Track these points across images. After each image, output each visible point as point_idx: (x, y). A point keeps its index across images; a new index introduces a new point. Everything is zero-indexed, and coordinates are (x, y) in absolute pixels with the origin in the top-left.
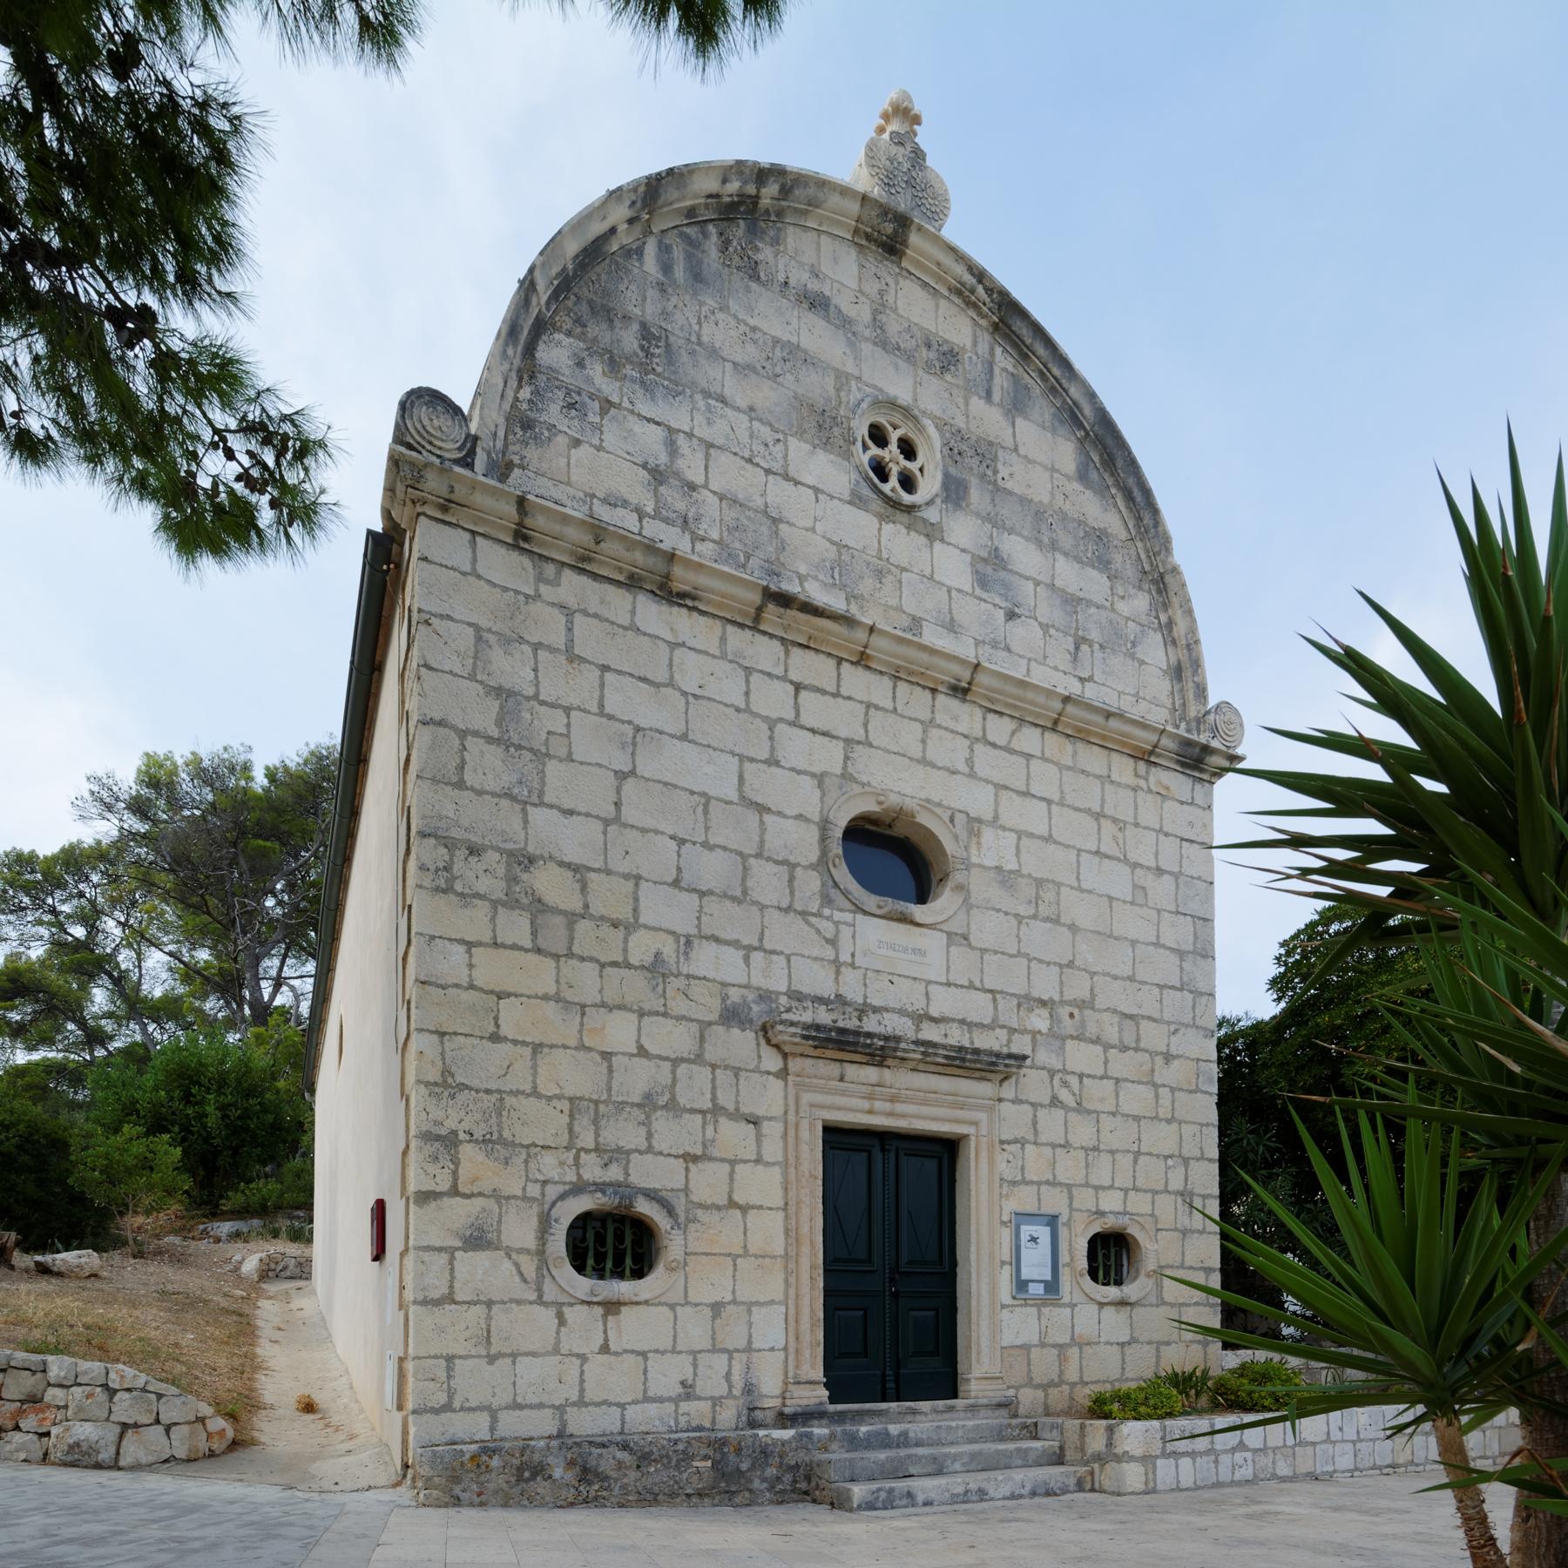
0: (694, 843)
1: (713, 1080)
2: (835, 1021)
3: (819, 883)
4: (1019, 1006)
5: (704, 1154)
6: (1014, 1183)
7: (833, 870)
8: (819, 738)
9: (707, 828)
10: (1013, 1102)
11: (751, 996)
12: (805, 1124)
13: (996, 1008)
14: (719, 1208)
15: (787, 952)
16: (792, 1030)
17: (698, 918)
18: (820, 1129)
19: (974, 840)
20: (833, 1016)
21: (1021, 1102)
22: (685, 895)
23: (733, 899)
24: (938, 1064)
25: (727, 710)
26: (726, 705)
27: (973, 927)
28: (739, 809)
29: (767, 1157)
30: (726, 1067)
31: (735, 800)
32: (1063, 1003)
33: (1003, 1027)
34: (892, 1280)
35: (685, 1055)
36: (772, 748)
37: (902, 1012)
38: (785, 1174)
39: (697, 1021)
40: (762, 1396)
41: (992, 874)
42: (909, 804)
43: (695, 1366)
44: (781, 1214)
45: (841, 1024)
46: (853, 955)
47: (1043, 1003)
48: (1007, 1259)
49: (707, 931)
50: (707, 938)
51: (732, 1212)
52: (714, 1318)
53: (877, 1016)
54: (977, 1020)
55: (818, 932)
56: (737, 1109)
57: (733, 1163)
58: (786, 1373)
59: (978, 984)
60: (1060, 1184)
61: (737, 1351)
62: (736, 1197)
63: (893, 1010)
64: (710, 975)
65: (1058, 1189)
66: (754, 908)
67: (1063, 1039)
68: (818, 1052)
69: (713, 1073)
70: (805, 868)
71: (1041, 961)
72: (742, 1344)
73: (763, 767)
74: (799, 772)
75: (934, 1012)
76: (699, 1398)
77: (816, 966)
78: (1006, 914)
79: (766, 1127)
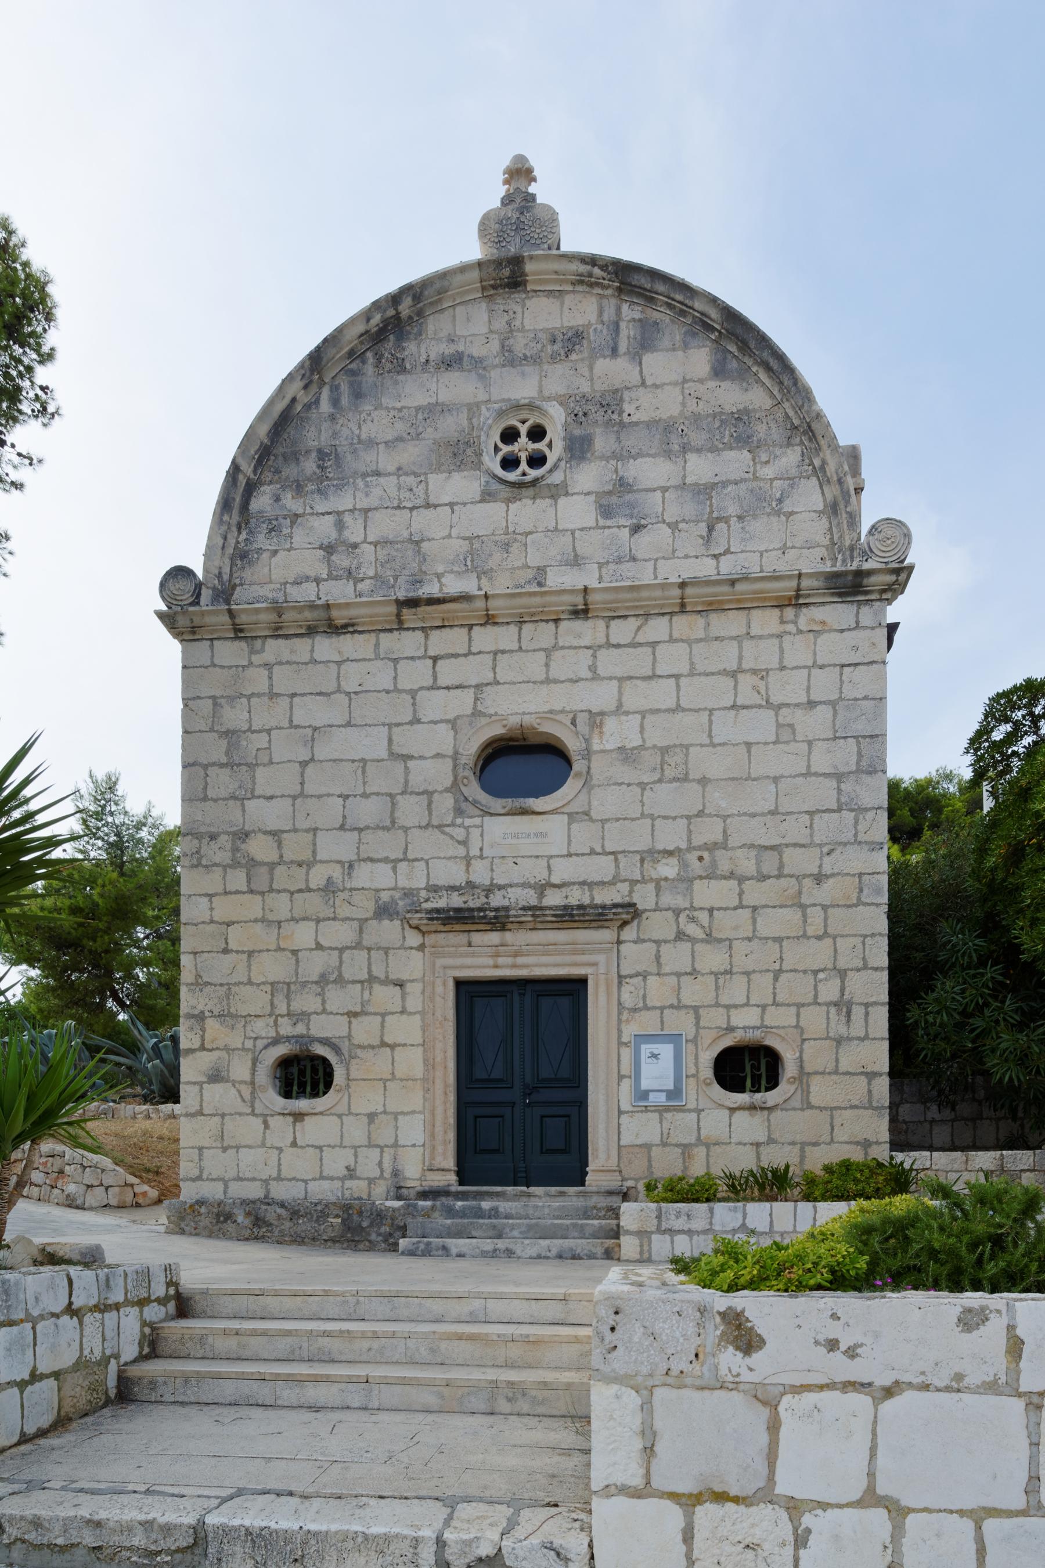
2: (465, 902)
14: (373, 1047)
16: (418, 915)
30: (379, 949)
37: (525, 885)
47: (670, 853)
50: (364, 860)
52: (369, 1124)
54: (597, 878)
55: (452, 837)
60: (685, 1007)
61: (387, 1146)
72: (391, 1141)
74: (435, 723)
76: (359, 1178)
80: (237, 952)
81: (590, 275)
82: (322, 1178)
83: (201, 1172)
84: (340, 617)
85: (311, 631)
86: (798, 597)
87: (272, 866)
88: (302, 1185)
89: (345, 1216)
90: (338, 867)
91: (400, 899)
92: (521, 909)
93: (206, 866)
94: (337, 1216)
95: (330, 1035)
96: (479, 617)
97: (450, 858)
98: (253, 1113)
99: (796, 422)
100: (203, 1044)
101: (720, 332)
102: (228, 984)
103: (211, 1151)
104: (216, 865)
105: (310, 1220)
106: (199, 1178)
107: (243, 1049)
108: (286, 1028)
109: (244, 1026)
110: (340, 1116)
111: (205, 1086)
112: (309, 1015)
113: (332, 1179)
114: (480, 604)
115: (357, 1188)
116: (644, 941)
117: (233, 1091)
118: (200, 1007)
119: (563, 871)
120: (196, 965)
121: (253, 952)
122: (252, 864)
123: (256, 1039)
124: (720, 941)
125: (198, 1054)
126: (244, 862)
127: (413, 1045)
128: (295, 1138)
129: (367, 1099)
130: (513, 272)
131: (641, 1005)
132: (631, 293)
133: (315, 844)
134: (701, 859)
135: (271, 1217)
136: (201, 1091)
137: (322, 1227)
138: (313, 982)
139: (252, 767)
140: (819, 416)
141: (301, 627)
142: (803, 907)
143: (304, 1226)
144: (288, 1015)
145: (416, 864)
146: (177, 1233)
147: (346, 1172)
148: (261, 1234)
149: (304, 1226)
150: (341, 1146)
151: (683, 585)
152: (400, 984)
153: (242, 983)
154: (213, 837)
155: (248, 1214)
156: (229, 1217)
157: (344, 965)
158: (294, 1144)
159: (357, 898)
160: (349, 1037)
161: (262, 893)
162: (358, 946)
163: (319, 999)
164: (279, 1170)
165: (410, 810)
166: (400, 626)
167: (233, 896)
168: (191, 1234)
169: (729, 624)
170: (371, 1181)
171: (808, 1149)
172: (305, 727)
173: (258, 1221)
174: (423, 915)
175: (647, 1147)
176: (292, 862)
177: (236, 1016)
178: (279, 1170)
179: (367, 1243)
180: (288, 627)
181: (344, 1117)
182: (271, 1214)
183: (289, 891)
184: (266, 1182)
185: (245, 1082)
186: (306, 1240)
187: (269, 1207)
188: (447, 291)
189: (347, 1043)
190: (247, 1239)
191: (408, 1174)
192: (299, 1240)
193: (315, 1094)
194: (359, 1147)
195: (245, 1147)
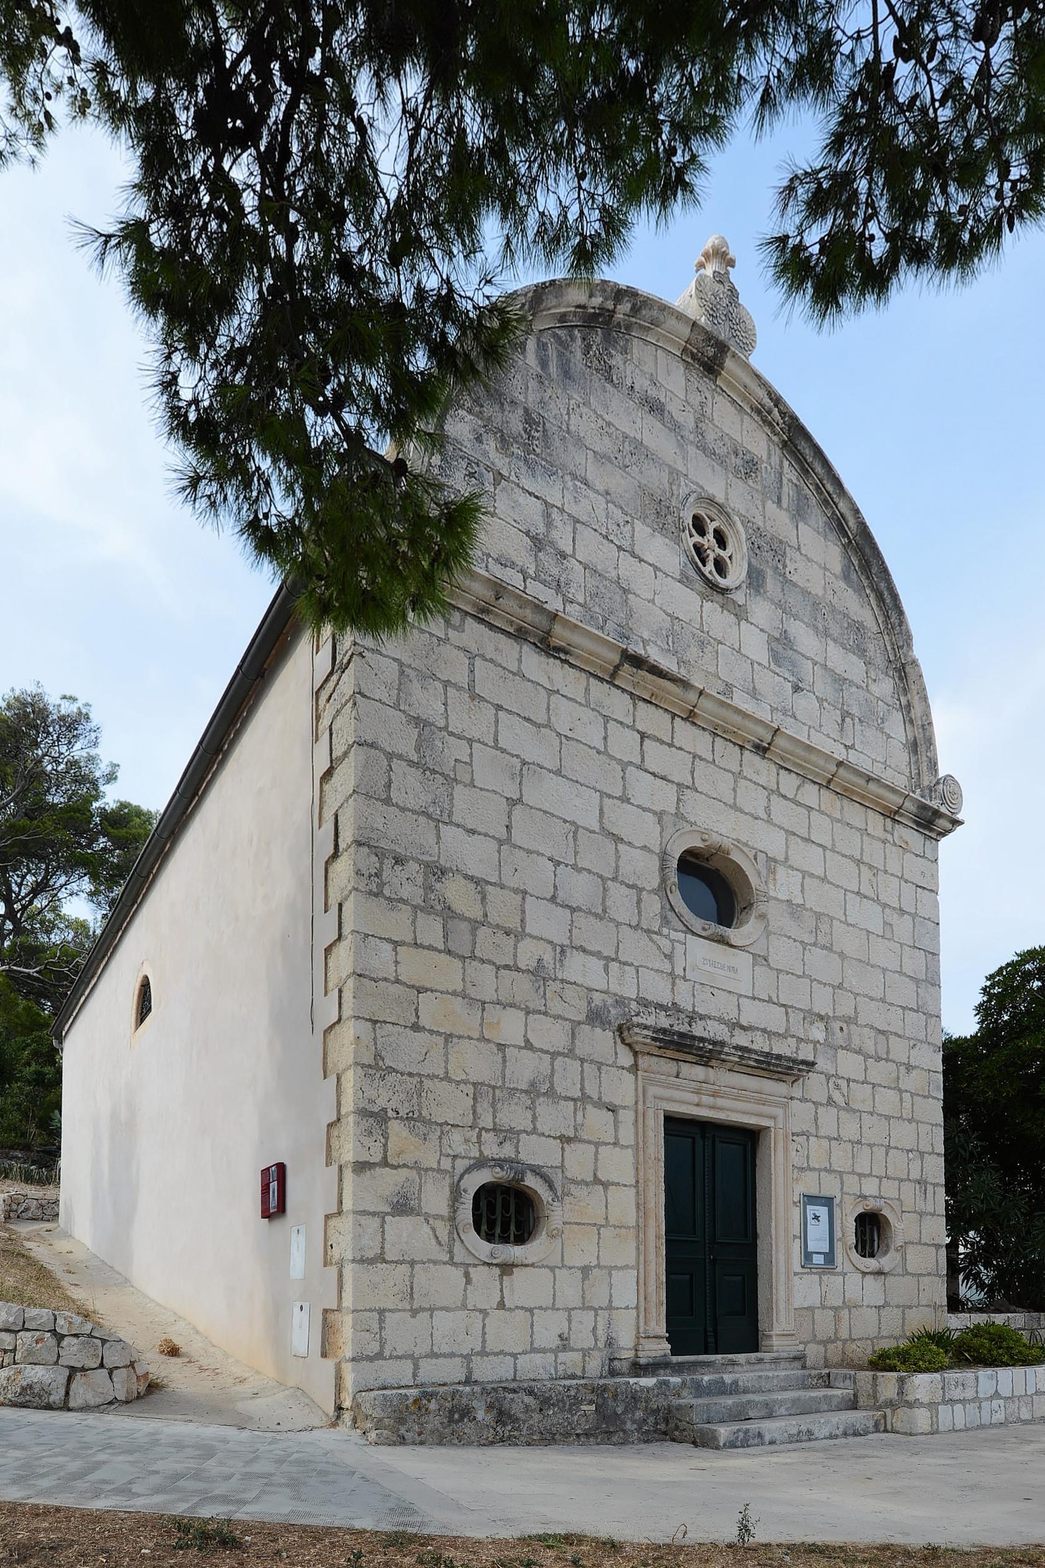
2: (671, 1026)
14: (587, 1184)
16: (645, 1032)
30: (592, 1061)
35: (561, 1050)
37: (721, 1020)
44: (633, 1190)
47: (821, 1018)
50: (576, 948)
52: (583, 1280)
54: (774, 1030)
55: (659, 948)
59: (775, 1000)
60: (834, 1171)
61: (601, 1308)
72: (605, 1304)
74: (644, 810)
76: (573, 1350)
80: (431, 1032)
81: (770, 412)
82: (534, 1350)
83: (382, 1346)
84: (560, 635)
85: (520, 635)
86: (896, 813)
87: (475, 925)
88: (509, 1360)
89: (600, 1401)
90: (549, 947)
91: (612, 1005)
92: (734, 1047)
93: (389, 899)
94: (591, 1402)
95: (541, 1164)
96: (682, 709)
97: (657, 971)
98: (451, 1262)
99: (892, 658)
100: (385, 1157)
101: (850, 542)
102: (419, 1075)
103: (397, 1315)
104: (401, 900)
105: (562, 1410)
106: (379, 1356)
107: (439, 1171)
108: (491, 1149)
109: (440, 1138)
110: (552, 1269)
111: (388, 1218)
112: (519, 1133)
113: (544, 1351)
114: (692, 697)
115: (571, 1360)
116: (807, 1100)
117: (426, 1229)
118: (381, 1102)
119: (751, 1014)
120: (375, 1039)
121: (451, 1035)
122: (448, 914)
123: (455, 1157)
124: (855, 1111)
125: (379, 1171)
126: (439, 908)
127: (625, 1186)
128: (502, 1298)
129: (581, 1251)
130: (715, 355)
131: (805, 1165)
132: (792, 453)
133: (523, 912)
134: (841, 1029)
135: (517, 1410)
136: (382, 1226)
137: (576, 1418)
138: (522, 1091)
139: (451, 781)
140: (914, 662)
141: (511, 623)
142: (900, 1090)
143: (555, 1417)
144: (494, 1130)
145: (627, 968)
146: (394, 1444)
147: (558, 1342)
148: (507, 1434)
149: (555, 1417)
150: (554, 1308)
151: (840, 764)
152: (612, 1109)
153: (437, 1077)
154: (399, 861)
155: (490, 1407)
156: (466, 1413)
157: (556, 1075)
158: (501, 1305)
159: (570, 992)
160: (562, 1167)
161: (463, 958)
162: (570, 1053)
163: (529, 1114)
164: (484, 1341)
165: (621, 902)
166: (611, 679)
167: (426, 952)
168: (414, 1443)
169: (854, 814)
170: (586, 1353)
171: (907, 1311)
172: (513, 756)
173: (502, 1416)
174: (650, 1034)
175: (811, 1309)
176: (498, 926)
177: (428, 1122)
178: (484, 1341)
179: (621, 1434)
180: (497, 615)
181: (557, 1270)
182: (518, 1404)
183: (494, 964)
184: (467, 1358)
185: (442, 1217)
186: (557, 1437)
187: (515, 1395)
188: (657, 326)
189: (560, 1175)
190: (492, 1443)
191: (622, 1344)
192: (548, 1439)
193: (522, 1239)
194: (573, 1309)
195: (441, 1309)
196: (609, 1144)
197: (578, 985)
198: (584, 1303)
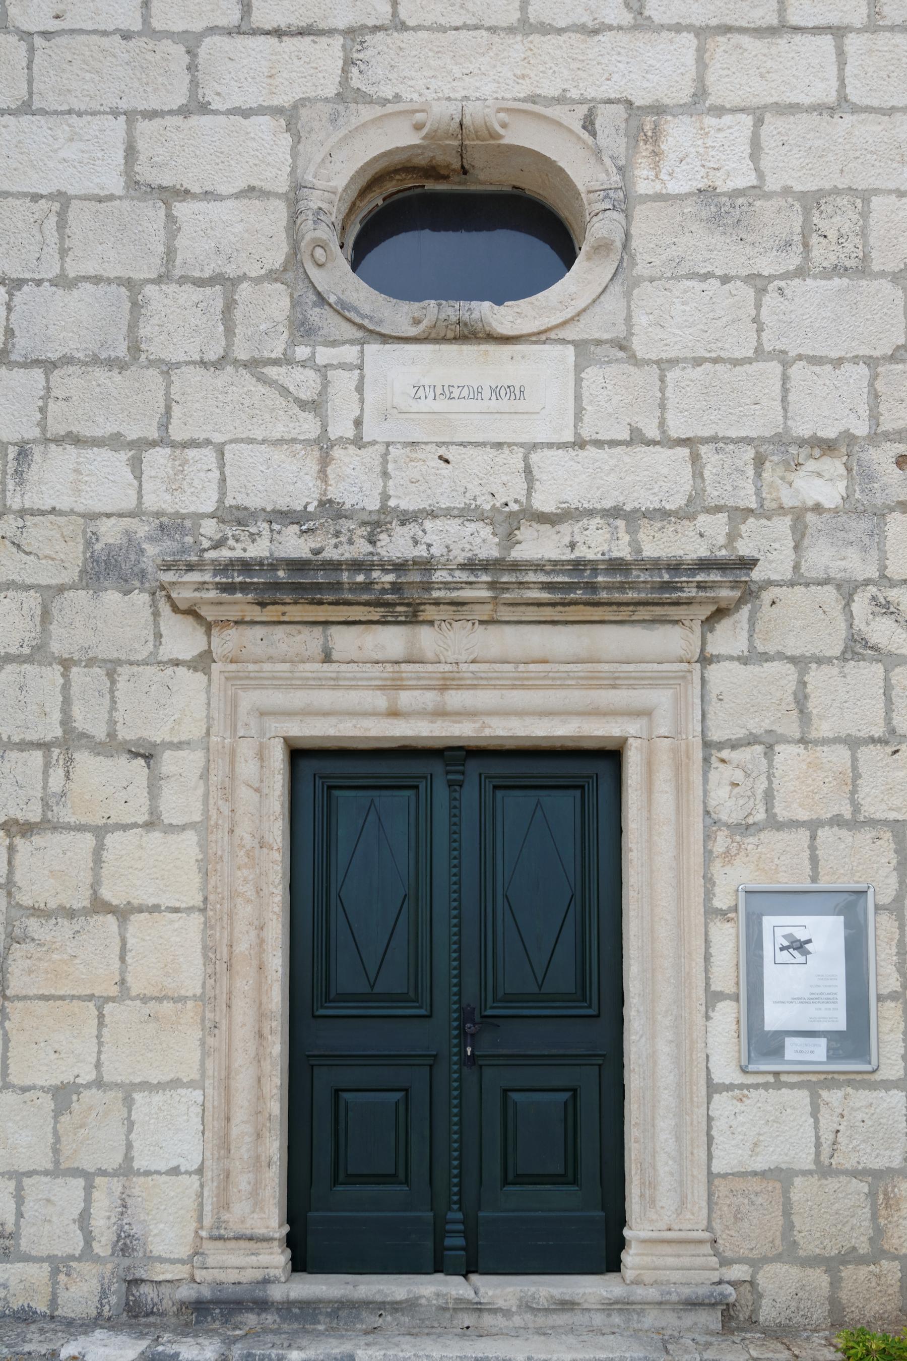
0: (39, 283)
1: (66, 687)
2: (317, 552)
3: (286, 302)
4: (759, 462)
5: (45, 820)
6: (745, 828)
7: (313, 272)
8: (289, 43)
9: (63, 252)
10: (744, 660)
11: (143, 530)
12: (246, 749)
13: (698, 474)
14: (71, 914)
15: (218, 438)
16: (195, 577)
17: (42, 410)
18: (278, 758)
19: (644, 149)
20: (313, 542)
21: (766, 657)
22: (19, 374)
23: (111, 363)
24: (539, 604)
25: (105, 42)
26: (105, 33)
27: (641, 320)
28: (126, 204)
29: (170, 815)
30: (91, 662)
31: (119, 191)
32: (876, 437)
33: (718, 509)
34: (463, 1034)
35: (13, 650)
36: (194, 84)
37: (467, 514)
38: (203, 846)
39: (37, 587)
40: (150, 1259)
41: (689, 207)
42: (475, 113)
43: (19, 1198)
44: (197, 920)
45: (331, 554)
46: (358, 423)
47: (827, 447)
48: (729, 988)
49: (56, 428)
50: (58, 441)
51: (100, 919)
52: (57, 1114)
53: (413, 529)
54: (649, 502)
55: (284, 391)
56: (112, 735)
57: (100, 832)
58: (200, 1219)
59: (652, 432)
60: (872, 823)
61: (103, 1173)
62: (106, 893)
63: (448, 513)
64: (64, 504)
65: (867, 835)
66: (152, 372)
67: (880, 514)
68: (272, 612)
69: (65, 675)
70: (258, 280)
71: (816, 360)
72: (114, 1160)
73: (177, 120)
74: (246, 113)
75: (544, 502)
76: (27, 1258)
77: (278, 455)
78: (725, 279)
79: (168, 762)
91: (150, 539)
127: (176, 910)
131: (760, 816)
174: (207, 577)
191: (158, 1248)
194: (30, 1174)
196: (135, 825)
197: (61, 513)
198: (57, 1163)
